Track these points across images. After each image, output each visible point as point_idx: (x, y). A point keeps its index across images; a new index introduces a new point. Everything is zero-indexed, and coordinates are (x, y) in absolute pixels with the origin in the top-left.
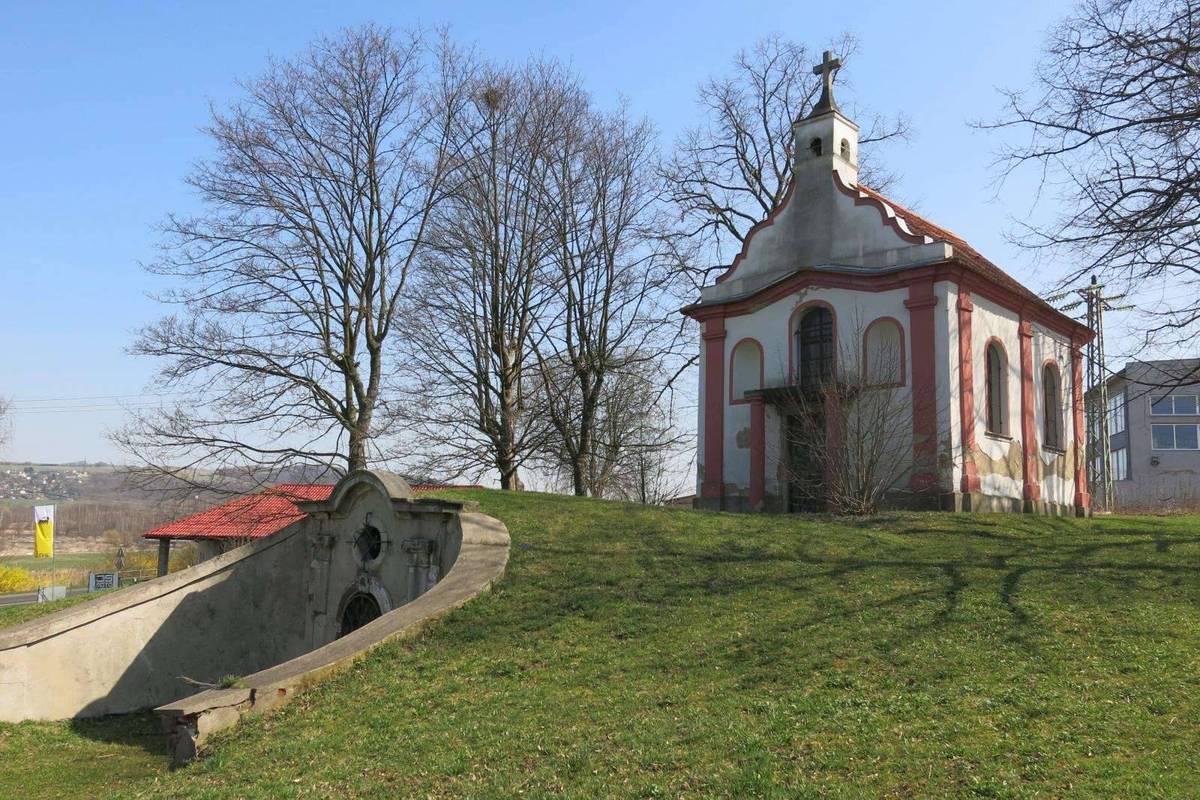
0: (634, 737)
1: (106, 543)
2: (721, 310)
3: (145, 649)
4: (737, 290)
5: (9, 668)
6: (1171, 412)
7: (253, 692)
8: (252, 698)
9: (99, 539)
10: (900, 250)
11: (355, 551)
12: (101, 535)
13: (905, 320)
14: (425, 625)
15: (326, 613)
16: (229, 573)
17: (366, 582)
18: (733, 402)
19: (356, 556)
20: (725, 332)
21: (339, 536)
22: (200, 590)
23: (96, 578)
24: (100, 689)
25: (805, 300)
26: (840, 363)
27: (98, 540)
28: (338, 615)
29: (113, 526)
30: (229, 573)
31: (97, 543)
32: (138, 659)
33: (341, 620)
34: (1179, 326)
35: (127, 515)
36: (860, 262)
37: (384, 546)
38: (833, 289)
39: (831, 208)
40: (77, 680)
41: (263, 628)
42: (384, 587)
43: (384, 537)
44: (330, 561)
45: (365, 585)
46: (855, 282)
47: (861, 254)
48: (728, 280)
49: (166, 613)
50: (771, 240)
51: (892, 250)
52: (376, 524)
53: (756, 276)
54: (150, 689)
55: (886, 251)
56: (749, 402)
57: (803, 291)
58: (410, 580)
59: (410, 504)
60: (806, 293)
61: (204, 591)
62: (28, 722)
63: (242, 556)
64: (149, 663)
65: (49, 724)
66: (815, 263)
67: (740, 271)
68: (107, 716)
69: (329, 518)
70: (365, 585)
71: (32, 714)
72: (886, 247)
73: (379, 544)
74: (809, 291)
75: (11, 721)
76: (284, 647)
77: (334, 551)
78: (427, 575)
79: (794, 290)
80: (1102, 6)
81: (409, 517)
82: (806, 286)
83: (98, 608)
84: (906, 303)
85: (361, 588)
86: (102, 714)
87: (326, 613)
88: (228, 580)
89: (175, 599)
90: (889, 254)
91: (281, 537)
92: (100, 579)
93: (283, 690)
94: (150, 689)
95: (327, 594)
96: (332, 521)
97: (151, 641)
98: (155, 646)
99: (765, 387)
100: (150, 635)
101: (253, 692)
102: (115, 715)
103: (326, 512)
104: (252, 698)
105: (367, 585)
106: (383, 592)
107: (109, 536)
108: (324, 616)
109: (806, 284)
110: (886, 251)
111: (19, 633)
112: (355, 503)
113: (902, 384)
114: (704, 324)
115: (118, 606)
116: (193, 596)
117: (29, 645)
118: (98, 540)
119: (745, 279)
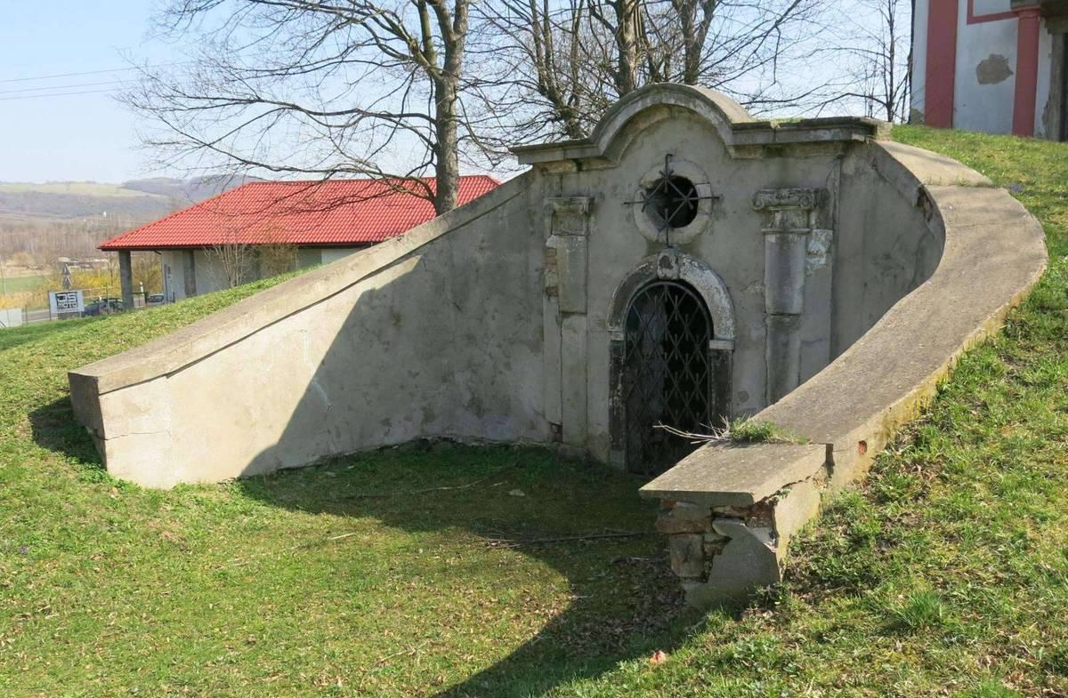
1: (18, 266)
3: (316, 374)
5: (147, 410)
7: (829, 449)
8: (829, 464)
9: (10, 263)
11: (640, 216)
12: (11, 258)
15: (585, 314)
16: (415, 260)
17: (673, 264)
18: (972, 20)
19: (645, 226)
21: (602, 196)
22: (378, 287)
23: (57, 297)
24: (266, 429)
27: (8, 264)
28: (616, 312)
29: (22, 248)
30: (415, 260)
31: (8, 266)
32: (309, 389)
33: (623, 319)
35: (34, 235)
37: (705, 206)
40: (237, 423)
41: (470, 338)
42: (710, 268)
43: (703, 191)
44: (588, 236)
49: (338, 322)
52: (682, 170)
54: (329, 432)
58: (769, 257)
59: (775, 131)
61: (383, 288)
62: (185, 488)
63: (433, 235)
64: (325, 396)
65: (210, 488)
68: (280, 472)
69: (580, 169)
70: (671, 268)
71: (189, 478)
73: (695, 203)
75: (163, 488)
76: (508, 365)
77: (593, 218)
78: (807, 246)
80: (235, 2)
81: (759, 155)
83: (251, 317)
85: (661, 273)
86: (273, 470)
87: (585, 314)
88: (415, 271)
89: (347, 302)
91: (489, 204)
92: (62, 298)
93: (863, 444)
94: (329, 432)
95: (586, 285)
96: (582, 175)
97: (323, 362)
98: (329, 371)
100: (321, 357)
101: (829, 449)
102: (288, 469)
103: (575, 160)
104: (829, 464)
106: (712, 279)
107: (19, 258)
108: (583, 319)
111: (153, 358)
112: (634, 142)
115: (277, 315)
116: (370, 296)
117: (168, 375)
118: (8, 264)
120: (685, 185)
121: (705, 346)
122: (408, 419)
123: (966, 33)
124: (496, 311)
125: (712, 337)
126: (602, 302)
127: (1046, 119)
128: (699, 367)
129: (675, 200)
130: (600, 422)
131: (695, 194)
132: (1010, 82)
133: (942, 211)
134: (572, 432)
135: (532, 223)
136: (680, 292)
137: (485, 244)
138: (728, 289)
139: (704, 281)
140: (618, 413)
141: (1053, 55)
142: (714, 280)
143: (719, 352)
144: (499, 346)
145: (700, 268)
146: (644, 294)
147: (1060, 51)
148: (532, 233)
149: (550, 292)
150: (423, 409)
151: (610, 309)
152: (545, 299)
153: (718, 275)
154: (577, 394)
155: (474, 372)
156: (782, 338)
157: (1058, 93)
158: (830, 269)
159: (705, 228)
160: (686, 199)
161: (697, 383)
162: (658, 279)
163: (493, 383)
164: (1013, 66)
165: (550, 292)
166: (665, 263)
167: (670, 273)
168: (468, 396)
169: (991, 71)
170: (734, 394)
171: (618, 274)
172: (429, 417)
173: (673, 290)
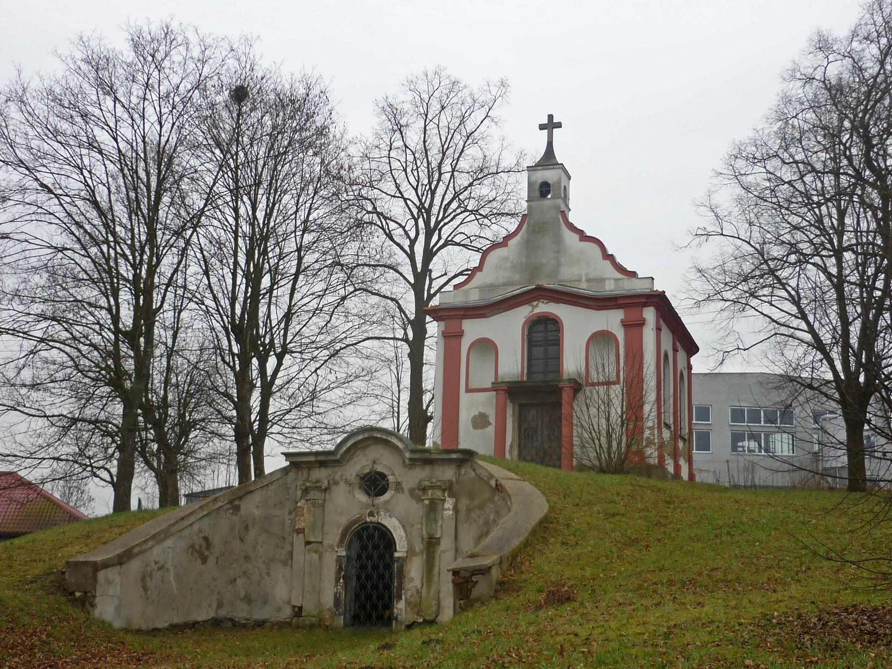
0: (527, 632)
2: (462, 313)
4: (474, 297)
6: (697, 420)
10: (616, 280)
13: (620, 334)
14: (439, 544)
17: (375, 515)
18: (468, 390)
20: (463, 332)
25: (536, 311)
26: (565, 366)
34: (745, 350)
36: (584, 285)
37: (392, 486)
38: (561, 304)
39: (558, 240)
41: (247, 558)
43: (391, 478)
45: (374, 516)
46: (580, 301)
47: (584, 279)
48: (466, 287)
50: (506, 259)
51: (610, 279)
53: (491, 287)
55: (605, 279)
56: (495, 390)
57: (535, 303)
60: (537, 306)
66: (546, 284)
67: (478, 280)
68: (154, 630)
70: (374, 516)
72: (605, 276)
73: (388, 485)
74: (540, 304)
76: (268, 574)
79: (528, 302)
82: (538, 300)
84: (622, 321)
90: (607, 281)
99: (499, 380)
105: (376, 517)
109: (537, 299)
110: (605, 279)
112: (354, 453)
113: (617, 382)
114: (442, 324)
119: (481, 288)
120: (383, 476)
121: (392, 554)
122: (210, 606)
123: (465, 398)
124: (263, 542)
125: (396, 551)
126: (333, 536)
127: (511, 452)
128: (388, 567)
129: (378, 483)
130: (328, 600)
131: (388, 480)
132: (491, 430)
133: (508, 489)
134: (309, 607)
135: (288, 494)
136: (379, 529)
137: (260, 505)
138: (404, 527)
139: (392, 524)
140: (340, 595)
141: (513, 415)
142: (397, 523)
143: (399, 558)
144: (264, 563)
145: (390, 516)
146: (358, 531)
147: (517, 414)
148: (288, 499)
149: (300, 531)
150: (218, 600)
151: (338, 538)
152: (295, 535)
153: (399, 520)
154: (314, 587)
155: (248, 578)
156: (432, 550)
157: (516, 437)
158: (454, 516)
159: (392, 497)
160: (383, 482)
161: (387, 576)
162: (366, 522)
163: (259, 584)
164: (492, 419)
165: (300, 531)
166: (371, 514)
167: (374, 519)
168: (242, 594)
169: (480, 421)
170: (406, 579)
171: (344, 521)
172: (220, 605)
173: (375, 528)
